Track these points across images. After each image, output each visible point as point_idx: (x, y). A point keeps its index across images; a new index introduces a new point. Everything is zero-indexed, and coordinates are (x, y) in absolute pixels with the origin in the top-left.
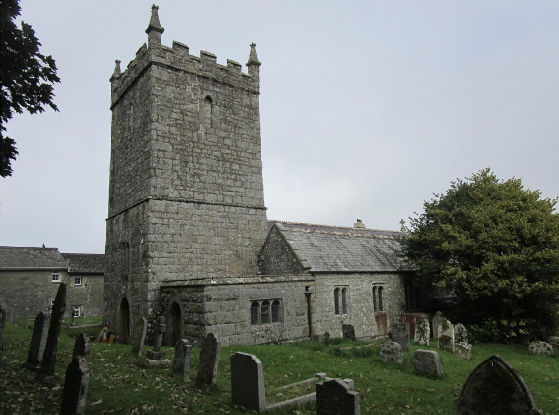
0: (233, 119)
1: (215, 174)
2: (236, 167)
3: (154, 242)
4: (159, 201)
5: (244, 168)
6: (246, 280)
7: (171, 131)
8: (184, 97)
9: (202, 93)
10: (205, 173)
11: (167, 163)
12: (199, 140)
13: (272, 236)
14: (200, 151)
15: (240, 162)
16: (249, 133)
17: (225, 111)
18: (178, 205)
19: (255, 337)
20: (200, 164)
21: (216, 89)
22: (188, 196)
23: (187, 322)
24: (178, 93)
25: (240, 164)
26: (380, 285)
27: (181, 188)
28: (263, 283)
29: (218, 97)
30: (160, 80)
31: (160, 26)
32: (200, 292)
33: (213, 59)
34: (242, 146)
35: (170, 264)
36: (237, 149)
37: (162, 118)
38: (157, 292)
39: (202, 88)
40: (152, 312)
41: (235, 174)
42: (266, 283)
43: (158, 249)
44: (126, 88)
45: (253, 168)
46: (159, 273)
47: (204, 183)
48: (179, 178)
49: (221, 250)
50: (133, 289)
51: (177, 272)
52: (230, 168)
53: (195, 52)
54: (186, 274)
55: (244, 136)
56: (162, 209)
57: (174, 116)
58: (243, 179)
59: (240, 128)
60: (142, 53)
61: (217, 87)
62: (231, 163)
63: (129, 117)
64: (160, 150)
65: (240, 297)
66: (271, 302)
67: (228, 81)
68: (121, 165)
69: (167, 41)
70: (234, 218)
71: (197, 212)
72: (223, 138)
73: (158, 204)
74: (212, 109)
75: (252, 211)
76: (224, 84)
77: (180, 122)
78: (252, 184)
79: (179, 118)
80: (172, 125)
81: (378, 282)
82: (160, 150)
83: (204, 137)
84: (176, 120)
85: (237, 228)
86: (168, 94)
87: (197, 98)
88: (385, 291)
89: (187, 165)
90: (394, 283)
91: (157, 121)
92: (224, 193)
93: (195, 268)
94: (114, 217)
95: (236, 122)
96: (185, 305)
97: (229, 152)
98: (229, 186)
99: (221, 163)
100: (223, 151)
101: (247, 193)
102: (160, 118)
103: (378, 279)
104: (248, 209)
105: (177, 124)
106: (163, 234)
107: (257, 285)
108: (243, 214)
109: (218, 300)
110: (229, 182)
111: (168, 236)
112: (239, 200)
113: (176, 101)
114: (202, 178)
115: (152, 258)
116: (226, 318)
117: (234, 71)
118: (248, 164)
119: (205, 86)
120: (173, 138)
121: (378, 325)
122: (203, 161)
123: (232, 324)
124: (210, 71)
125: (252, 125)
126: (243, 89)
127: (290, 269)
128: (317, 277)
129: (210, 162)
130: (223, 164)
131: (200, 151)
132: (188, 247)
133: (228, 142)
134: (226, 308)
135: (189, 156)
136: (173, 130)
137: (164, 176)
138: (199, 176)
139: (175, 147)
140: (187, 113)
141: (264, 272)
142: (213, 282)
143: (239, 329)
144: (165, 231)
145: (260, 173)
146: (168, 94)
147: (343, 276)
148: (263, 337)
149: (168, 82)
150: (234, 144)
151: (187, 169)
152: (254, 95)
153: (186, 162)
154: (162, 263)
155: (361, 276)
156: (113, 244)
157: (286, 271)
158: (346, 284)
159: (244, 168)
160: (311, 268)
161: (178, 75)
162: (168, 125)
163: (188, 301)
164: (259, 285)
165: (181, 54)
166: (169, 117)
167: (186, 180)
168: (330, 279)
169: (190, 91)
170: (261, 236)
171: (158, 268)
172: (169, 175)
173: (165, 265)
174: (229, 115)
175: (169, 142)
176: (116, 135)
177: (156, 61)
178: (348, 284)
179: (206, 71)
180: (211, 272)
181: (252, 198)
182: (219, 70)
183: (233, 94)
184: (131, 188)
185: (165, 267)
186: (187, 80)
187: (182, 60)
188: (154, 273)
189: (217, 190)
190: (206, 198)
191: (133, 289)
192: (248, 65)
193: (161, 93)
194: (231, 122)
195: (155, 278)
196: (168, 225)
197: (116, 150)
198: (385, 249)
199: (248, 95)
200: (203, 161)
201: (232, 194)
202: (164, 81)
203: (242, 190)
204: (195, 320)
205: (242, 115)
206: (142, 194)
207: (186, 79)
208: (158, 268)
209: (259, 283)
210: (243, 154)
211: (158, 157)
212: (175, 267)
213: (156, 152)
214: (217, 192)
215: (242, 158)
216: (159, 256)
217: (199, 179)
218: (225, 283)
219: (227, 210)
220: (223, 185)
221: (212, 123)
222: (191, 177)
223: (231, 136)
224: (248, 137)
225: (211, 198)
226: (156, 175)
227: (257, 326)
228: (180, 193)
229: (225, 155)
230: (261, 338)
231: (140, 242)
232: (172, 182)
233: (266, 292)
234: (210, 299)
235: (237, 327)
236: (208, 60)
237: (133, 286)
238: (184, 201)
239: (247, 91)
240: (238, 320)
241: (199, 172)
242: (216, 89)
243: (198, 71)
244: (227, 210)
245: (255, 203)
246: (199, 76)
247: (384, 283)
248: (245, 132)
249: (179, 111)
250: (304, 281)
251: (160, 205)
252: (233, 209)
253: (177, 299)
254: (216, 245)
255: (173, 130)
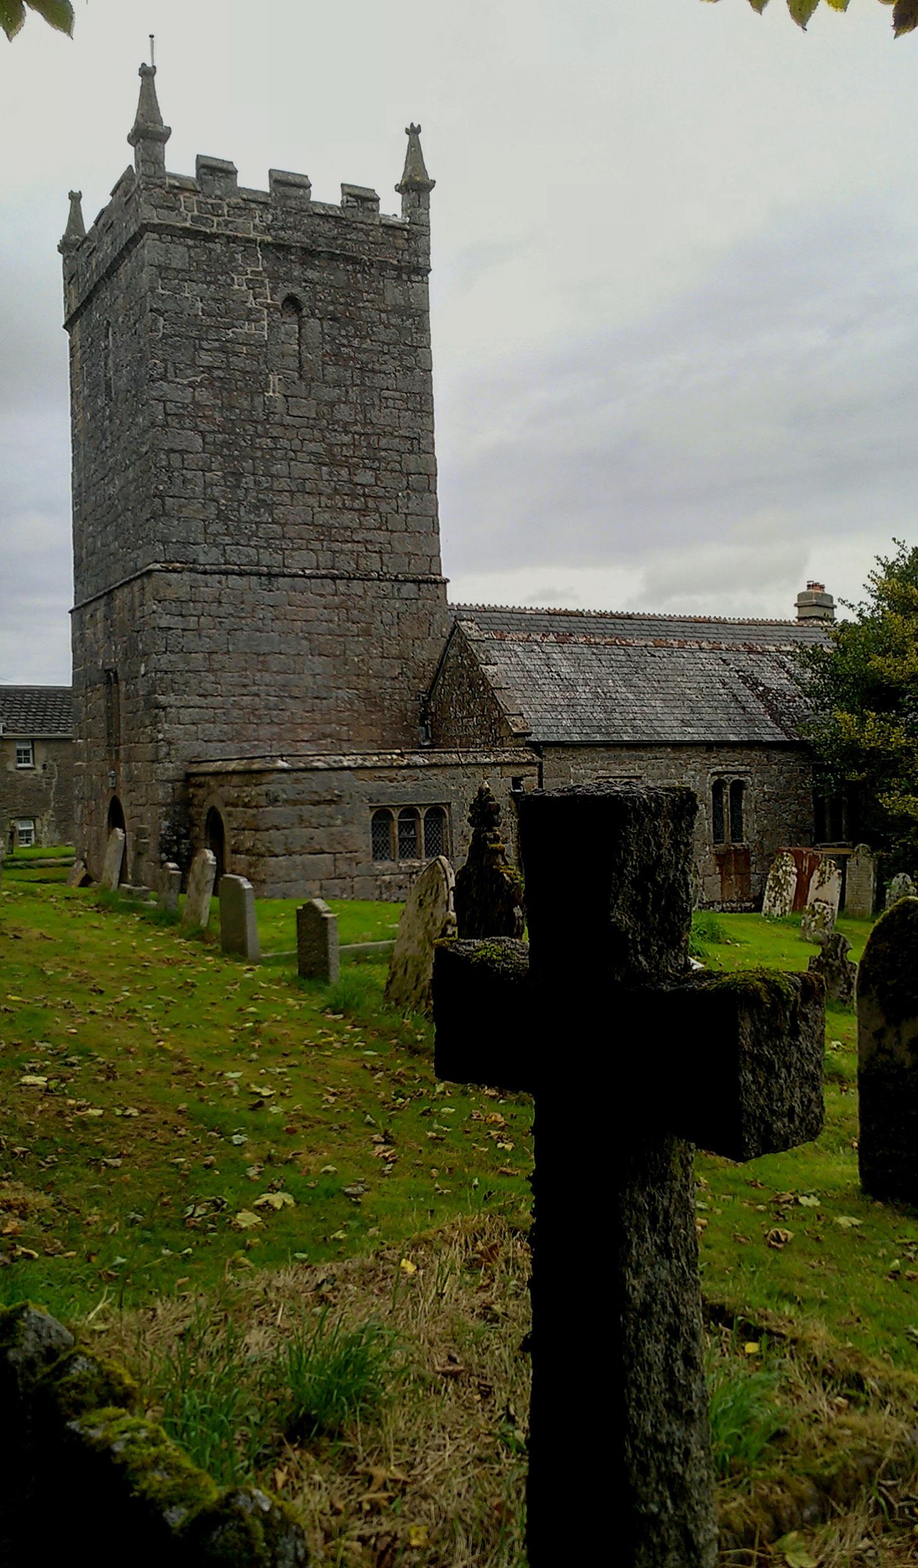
0: (358, 349)
1: (312, 500)
2: (366, 477)
3: (166, 672)
4: (175, 575)
5: (387, 479)
6: (360, 762)
7: (198, 398)
8: (228, 307)
9: (273, 291)
10: (285, 498)
11: (190, 481)
12: (268, 416)
13: (452, 652)
14: (271, 445)
15: (377, 464)
16: (401, 385)
17: (335, 332)
18: (219, 582)
19: (380, 887)
20: (272, 476)
21: (312, 274)
22: (245, 560)
23: (235, 851)
24: (213, 299)
25: (378, 469)
26: (736, 777)
27: (228, 540)
28: (400, 767)
29: (316, 293)
30: (167, 269)
31: (161, 121)
32: (256, 785)
33: (301, 192)
34: (382, 421)
35: (207, 721)
36: (369, 430)
37: (176, 368)
38: (179, 784)
39: (274, 277)
40: (168, 828)
41: (364, 495)
42: (408, 767)
43: (176, 687)
44: (95, 278)
45: (412, 478)
46: (182, 743)
47: (283, 525)
48: (221, 516)
49: (328, 687)
50: (130, 778)
51: (223, 741)
52: (351, 481)
53: (253, 178)
54: (245, 745)
55: (386, 393)
56: (184, 593)
57: (205, 359)
58: (384, 507)
59: (373, 371)
60: (124, 189)
61: (313, 268)
62: (352, 469)
63: (107, 357)
64: (173, 451)
65: (347, 799)
66: (423, 813)
67: (343, 248)
68: (95, 480)
69: (179, 162)
70: (361, 610)
71: (268, 597)
72: (332, 404)
73: (173, 582)
74: (300, 329)
75: (409, 589)
76: (333, 257)
77: (221, 373)
78: (409, 518)
79: (216, 364)
80: (201, 384)
81: (730, 769)
82: (173, 451)
83: (280, 407)
84: (210, 369)
85: (367, 633)
86: (186, 304)
87: (261, 304)
88: (752, 793)
89: (239, 481)
90: (781, 772)
91: (163, 378)
92: (336, 546)
93: (265, 731)
94: (85, 605)
95: (364, 357)
96: (230, 814)
97: (347, 439)
98: (346, 528)
99: (324, 468)
100: (333, 438)
101: (395, 543)
102: (171, 369)
103: (733, 766)
104: (397, 585)
105: (212, 380)
106: (186, 652)
107: (386, 773)
108: (385, 597)
109: (295, 803)
110: (347, 518)
111: (200, 656)
112: (373, 563)
113: (208, 321)
114: (278, 512)
115: (164, 708)
116: (314, 843)
117: (360, 216)
118: (398, 467)
119: (282, 270)
120: (205, 417)
121: (725, 874)
122: (279, 468)
123: (325, 855)
124: (295, 228)
125: (410, 362)
126: (383, 266)
127: (487, 736)
128: (551, 755)
129: (298, 469)
130: (330, 474)
131: (271, 445)
132: (246, 681)
133: (344, 412)
134: (313, 820)
135: (244, 458)
136: (203, 395)
137: (186, 512)
138: (271, 507)
139: (210, 438)
140: (238, 348)
141: (436, 742)
142: (281, 764)
143: (343, 868)
144: (192, 646)
145: (430, 488)
146: (186, 304)
147: (625, 753)
148: (400, 887)
149: (188, 271)
150: (360, 417)
151: (241, 493)
152: (414, 278)
153: (238, 475)
154: (187, 719)
155: (677, 755)
156: (85, 670)
157: (478, 741)
158: (632, 773)
159: (387, 479)
160: (529, 734)
161: (211, 250)
162: (191, 385)
163: (235, 805)
164: (392, 774)
165: (218, 192)
166: (193, 365)
167: (239, 521)
168: (585, 761)
169: (244, 288)
170: (428, 652)
171: (177, 731)
172: (197, 511)
173: (193, 724)
174: (345, 342)
175: (195, 429)
176: (81, 401)
177: (156, 221)
178: (639, 772)
179: (282, 228)
180: (303, 741)
181: (408, 554)
182: (317, 221)
183: (357, 282)
184: (116, 539)
185: (194, 728)
186: (236, 260)
187: (220, 207)
188: (170, 743)
189: (317, 539)
190: (288, 561)
191: (130, 778)
192: (399, 189)
193: (170, 305)
194: (352, 358)
195: (173, 752)
196: (198, 631)
197: (82, 438)
198: (774, 679)
199: (398, 277)
200: (279, 468)
201: (356, 547)
202: (179, 271)
203: (381, 536)
204: (249, 844)
205: (382, 338)
206: (138, 556)
207: (232, 259)
208: (177, 731)
209: (391, 767)
210: (384, 442)
211: (169, 468)
212: (215, 730)
213: (163, 456)
214: (316, 545)
215: (383, 453)
216: (179, 704)
217: (271, 514)
218: (309, 766)
219: (342, 589)
220: (332, 527)
221: (301, 367)
222: (250, 512)
223: (353, 396)
224: (397, 395)
225: (299, 561)
226: (165, 514)
227: (388, 864)
228: (224, 554)
229: (336, 450)
230: (395, 890)
231: (138, 671)
232: (206, 528)
233: (406, 790)
234: (276, 800)
235: (338, 863)
236: (288, 197)
237: (130, 772)
238: (233, 573)
239: (395, 268)
240: (341, 849)
241: (269, 497)
242: (312, 274)
243: (263, 232)
244: (342, 589)
245: (416, 568)
246: (265, 246)
247: (746, 773)
248: (391, 382)
249: (217, 344)
250: (508, 764)
251: (179, 584)
252: (357, 587)
253: (215, 801)
254: (314, 676)
255: (203, 395)
